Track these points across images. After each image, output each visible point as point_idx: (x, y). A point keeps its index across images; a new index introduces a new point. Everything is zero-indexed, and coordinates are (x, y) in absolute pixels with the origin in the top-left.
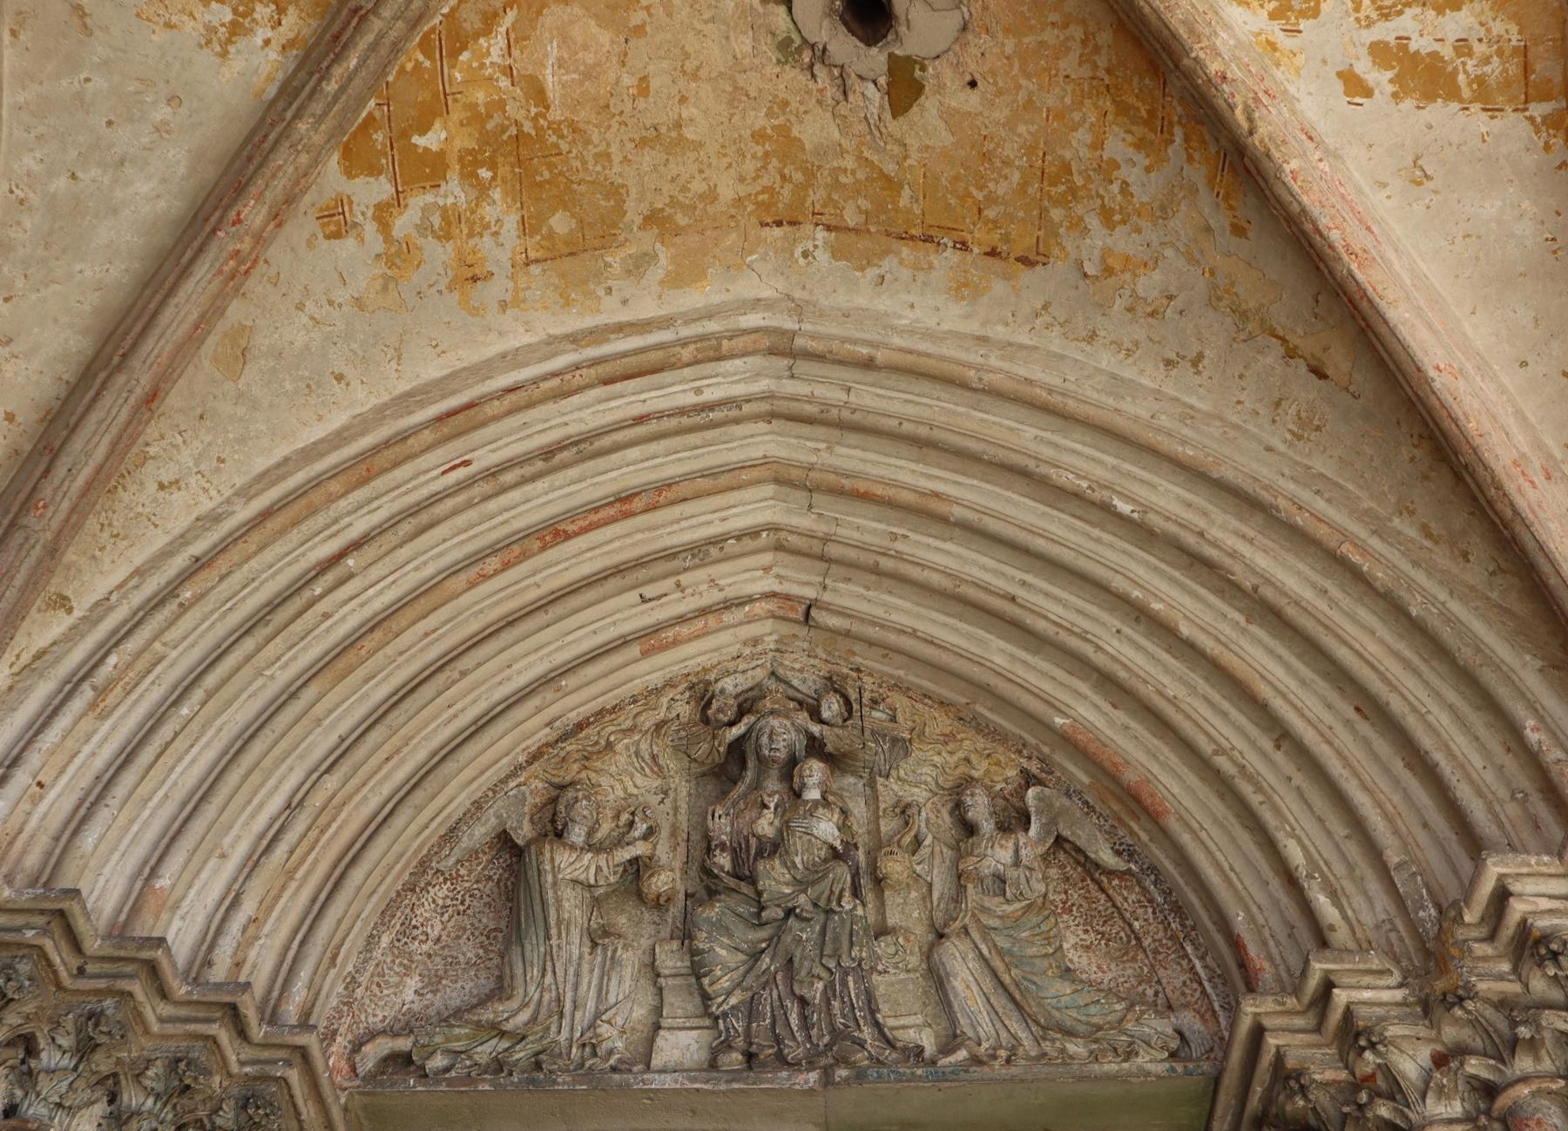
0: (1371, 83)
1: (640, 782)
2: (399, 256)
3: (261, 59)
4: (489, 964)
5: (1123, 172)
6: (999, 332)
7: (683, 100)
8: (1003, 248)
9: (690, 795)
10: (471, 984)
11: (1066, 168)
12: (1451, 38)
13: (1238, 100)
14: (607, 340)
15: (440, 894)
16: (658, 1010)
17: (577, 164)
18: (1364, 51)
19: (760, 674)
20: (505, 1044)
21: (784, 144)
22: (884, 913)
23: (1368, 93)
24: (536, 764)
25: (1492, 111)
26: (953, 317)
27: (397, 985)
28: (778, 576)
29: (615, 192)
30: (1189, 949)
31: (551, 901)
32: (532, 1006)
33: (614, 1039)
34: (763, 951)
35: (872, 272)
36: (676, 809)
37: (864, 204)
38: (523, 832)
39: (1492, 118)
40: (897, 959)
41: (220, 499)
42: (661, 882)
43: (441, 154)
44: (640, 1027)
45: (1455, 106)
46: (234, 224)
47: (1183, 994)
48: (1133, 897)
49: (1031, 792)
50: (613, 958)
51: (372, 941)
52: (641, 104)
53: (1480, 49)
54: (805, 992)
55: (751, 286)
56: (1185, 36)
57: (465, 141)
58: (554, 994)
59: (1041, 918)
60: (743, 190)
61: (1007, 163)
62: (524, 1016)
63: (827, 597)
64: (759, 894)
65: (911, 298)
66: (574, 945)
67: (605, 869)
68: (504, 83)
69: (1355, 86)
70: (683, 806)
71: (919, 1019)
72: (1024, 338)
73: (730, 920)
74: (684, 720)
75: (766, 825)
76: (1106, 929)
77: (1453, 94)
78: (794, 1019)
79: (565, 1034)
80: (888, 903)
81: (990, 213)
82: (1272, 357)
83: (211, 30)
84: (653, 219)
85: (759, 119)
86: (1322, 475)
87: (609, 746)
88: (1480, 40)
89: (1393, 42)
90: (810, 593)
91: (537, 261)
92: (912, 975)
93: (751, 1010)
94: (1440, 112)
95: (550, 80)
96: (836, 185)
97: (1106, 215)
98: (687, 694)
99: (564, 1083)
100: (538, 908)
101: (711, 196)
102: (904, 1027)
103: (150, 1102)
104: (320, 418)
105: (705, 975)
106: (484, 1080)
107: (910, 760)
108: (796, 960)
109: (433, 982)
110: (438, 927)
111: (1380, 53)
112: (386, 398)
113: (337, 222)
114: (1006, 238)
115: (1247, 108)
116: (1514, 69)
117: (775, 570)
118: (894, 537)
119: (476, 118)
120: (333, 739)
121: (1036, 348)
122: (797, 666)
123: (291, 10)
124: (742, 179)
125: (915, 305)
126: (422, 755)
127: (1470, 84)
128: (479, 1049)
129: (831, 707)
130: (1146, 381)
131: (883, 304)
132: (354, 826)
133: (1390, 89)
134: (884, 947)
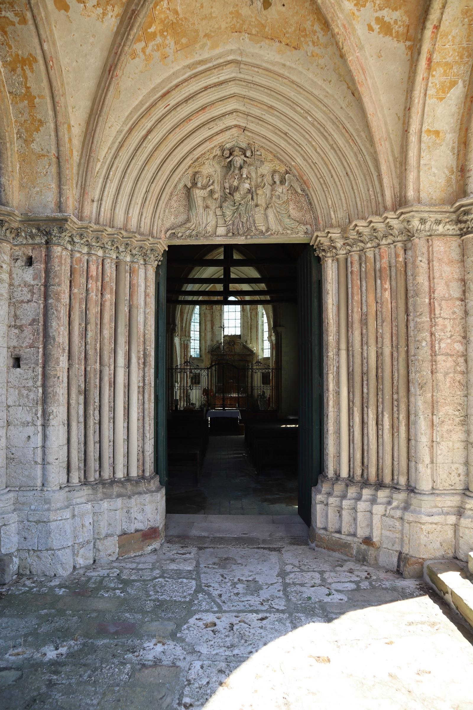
1: (211, 169)
2: (148, 58)
3: (111, 21)
5: (318, 34)
6: (288, 63)
7: (212, 7)
8: (290, 44)
11: (305, 29)
12: (394, 19)
13: (341, 40)
14: (197, 68)
16: (217, 222)
17: (187, 27)
18: (374, 19)
19: (234, 142)
21: (238, 14)
23: (373, 31)
25: (398, 41)
26: (278, 58)
29: (197, 31)
33: (209, 229)
35: (258, 45)
37: (257, 29)
38: (189, 185)
42: (216, 196)
43: (155, 32)
45: (391, 38)
51: (164, 211)
52: (201, 10)
53: (399, 23)
55: (229, 47)
57: (160, 27)
60: (227, 25)
61: (291, 25)
62: (194, 226)
63: (248, 126)
66: (201, 210)
68: (168, 12)
72: (293, 66)
75: (236, 183)
77: (391, 35)
81: (287, 35)
82: (345, 87)
83: (98, 15)
84: (206, 35)
85: (231, 9)
90: (244, 125)
93: (233, 224)
94: (388, 39)
95: (179, 9)
96: (250, 24)
97: (313, 43)
101: (220, 28)
109: (176, 217)
111: (377, 19)
113: (134, 55)
114: (290, 42)
116: (405, 31)
118: (262, 114)
119: (162, 21)
120: (152, 174)
123: (116, 6)
124: (227, 23)
125: (269, 54)
126: (168, 172)
129: (248, 154)
130: (319, 83)
131: (261, 52)
132: (158, 191)
134: (257, 209)
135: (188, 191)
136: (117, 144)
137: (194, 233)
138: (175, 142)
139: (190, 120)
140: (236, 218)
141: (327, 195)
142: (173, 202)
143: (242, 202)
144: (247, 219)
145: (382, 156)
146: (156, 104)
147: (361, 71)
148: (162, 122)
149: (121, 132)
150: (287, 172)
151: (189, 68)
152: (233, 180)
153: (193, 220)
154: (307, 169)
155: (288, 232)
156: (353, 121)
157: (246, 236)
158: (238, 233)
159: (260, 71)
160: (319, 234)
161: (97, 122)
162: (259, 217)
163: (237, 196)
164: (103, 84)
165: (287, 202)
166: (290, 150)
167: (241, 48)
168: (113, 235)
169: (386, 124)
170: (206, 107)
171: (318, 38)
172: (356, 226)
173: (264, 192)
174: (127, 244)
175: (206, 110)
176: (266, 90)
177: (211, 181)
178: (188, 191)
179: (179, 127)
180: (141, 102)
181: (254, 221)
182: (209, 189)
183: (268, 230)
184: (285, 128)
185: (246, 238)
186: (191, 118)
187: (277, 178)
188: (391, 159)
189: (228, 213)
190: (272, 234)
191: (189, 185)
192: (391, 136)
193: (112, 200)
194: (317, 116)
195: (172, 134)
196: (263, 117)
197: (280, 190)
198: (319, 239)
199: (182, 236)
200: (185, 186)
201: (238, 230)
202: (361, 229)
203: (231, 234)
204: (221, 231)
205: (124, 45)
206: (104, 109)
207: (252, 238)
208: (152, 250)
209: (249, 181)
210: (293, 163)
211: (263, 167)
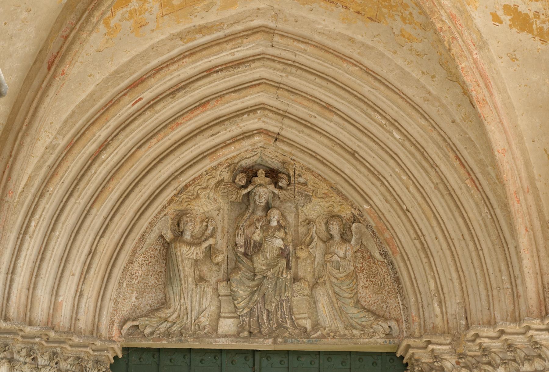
0: (502, 19)
1: (211, 205)
4: (160, 286)
5: (411, 9)
6: (359, 38)
9: (228, 210)
10: (154, 295)
12: (534, 10)
13: (446, 38)
14: (195, 39)
15: (140, 260)
16: (219, 307)
18: (501, 8)
19: (255, 158)
20: (169, 324)
22: (297, 269)
23: (501, 22)
24: (171, 205)
26: (340, 28)
27: (130, 298)
28: (264, 122)
30: (399, 296)
31: (181, 269)
32: (178, 311)
33: (204, 321)
34: (256, 291)
36: (223, 219)
38: (169, 236)
39: (542, 44)
40: (300, 292)
41: (52, 137)
42: (219, 258)
44: (213, 314)
45: (530, 36)
46: (62, 75)
47: (395, 310)
48: (384, 270)
49: (354, 225)
50: (203, 291)
53: (542, 17)
54: (268, 308)
56: (429, 14)
58: (185, 307)
59: (351, 281)
63: (283, 133)
64: (254, 269)
65: (324, 18)
67: (199, 253)
69: (496, 19)
70: (226, 216)
71: (306, 315)
73: (244, 280)
74: (226, 181)
75: (257, 237)
76: (374, 280)
77: (531, 31)
78: (265, 317)
79: (189, 320)
80: (299, 265)
86: (470, 138)
87: (198, 196)
88: (543, 14)
89: (512, 6)
90: (277, 130)
91: (167, 14)
92: (305, 297)
93: (251, 313)
94: (525, 36)
98: (227, 169)
99: (190, 341)
100: (177, 271)
102: (301, 318)
103: (69, 366)
104: (84, 91)
105: (236, 300)
106: (164, 339)
107: (311, 204)
108: (266, 295)
110: (141, 272)
112: (107, 74)
114: (364, 10)
115: (449, 42)
117: (263, 119)
120: (101, 219)
121: (373, 48)
122: (270, 156)
127: (537, 29)
128: (161, 326)
130: (414, 75)
131: (312, 16)
133: (509, 23)
134: (296, 286)
135: (166, 249)
136: (44, 169)
137: (175, 328)
138: (147, 161)
139: (178, 125)
140: (257, 302)
141: (428, 271)
142: (135, 267)
143: (269, 273)
144: (277, 306)
145: (520, 220)
146: (119, 100)
147: (481, 83)
148: (128, 130)
149: (54, 147)
150: (354, 219)
151: (181, 39)
152: (252, 229)
153: (175, 303)
154: (392, 217)
155: (355, 332)
156: (475, 146)
157: (275, 339)
158: (260, 332)
159: (310, 49)
160: (411, 342)
161: (21, 144)
162: (299, 302)
163: (260, 262)
164: (36, 83)
165: (354, 276)
166: (362, 179)
167: (276, 6)
168: (33, 338)
169: (527, 164)
170: (208, 102)
171: (411, 13)
172: (477, 336)
173: (310, 254)
174: (55, 353)
175: (208, 106)
176: (318, 80)
177: (211, 228)
178: (166, 249)
179: (157, 137)
180: (91, 95)
181: (291, 309)
182: (205, 245)
183: (316, 326)
184: (353, 144)
185: (275, 342)
186: (179, 121)
187: (335, 229)
188: (537, 224)
189: (242, 292)
190: (323, 336)
191: (169, 236)
192: (538, 184)
193: (29, 270)
194: (409, 129)
195: (143, 150)
196: (313, 120)
197: (341, 253)
198: (411, 351)
199: (152, 333)
200: (162, 236)
201: (259, 325)
202: (486, 342)
203: (246, 334)
204: (227, 325)
205: (80, 30)
206: (36, 125)
207: (285, 342)
208: (97, 362)
209: (282, 234)
210: (366, 207)
211: (310, 206)
